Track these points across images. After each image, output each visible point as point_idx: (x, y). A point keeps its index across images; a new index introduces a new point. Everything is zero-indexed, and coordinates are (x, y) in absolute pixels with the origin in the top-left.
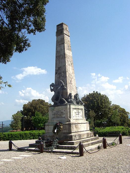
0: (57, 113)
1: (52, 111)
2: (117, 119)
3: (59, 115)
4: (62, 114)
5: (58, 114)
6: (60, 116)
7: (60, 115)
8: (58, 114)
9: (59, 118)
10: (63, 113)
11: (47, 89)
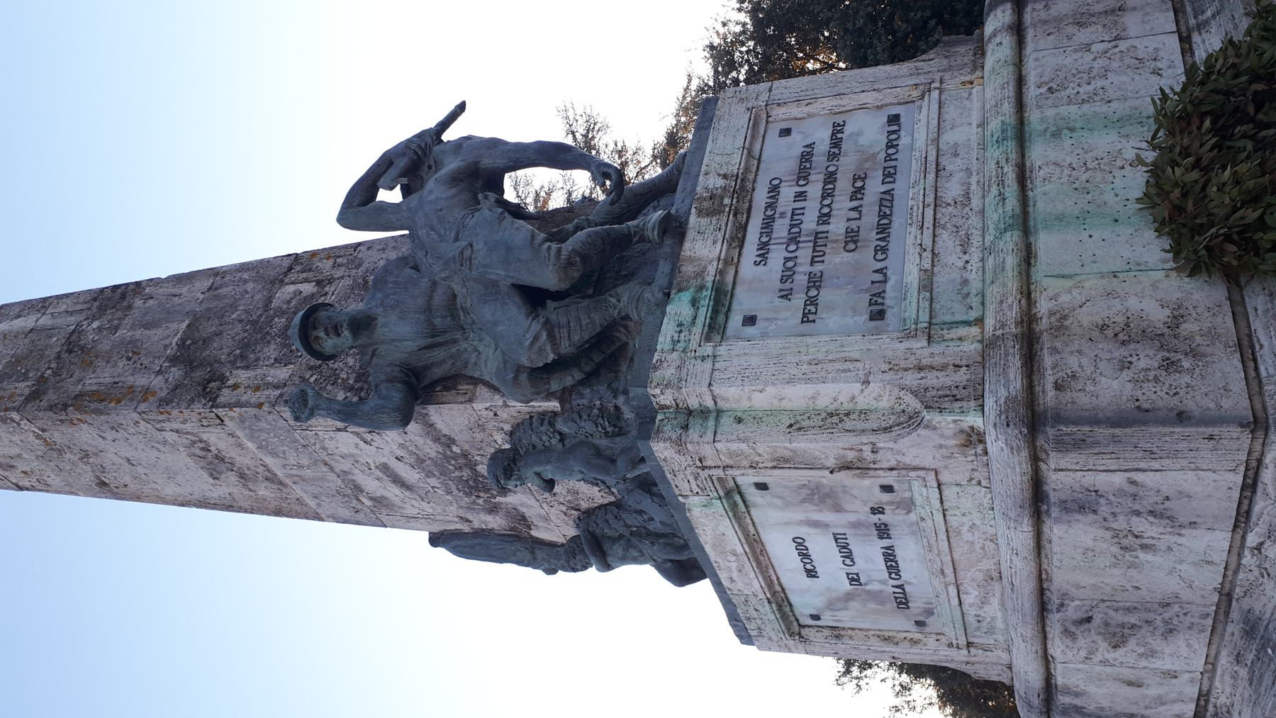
0: (794, 239)
1: (736, 320)
2: (478, 548)
3: (842, 204)
4: (832, 156)
5: (810, 222)
6: (857, 193)
7: (843, 185)
8: (824, 218)
9: (887, 200)
10: (823, 145)
11: (600, 196)
